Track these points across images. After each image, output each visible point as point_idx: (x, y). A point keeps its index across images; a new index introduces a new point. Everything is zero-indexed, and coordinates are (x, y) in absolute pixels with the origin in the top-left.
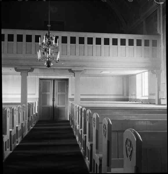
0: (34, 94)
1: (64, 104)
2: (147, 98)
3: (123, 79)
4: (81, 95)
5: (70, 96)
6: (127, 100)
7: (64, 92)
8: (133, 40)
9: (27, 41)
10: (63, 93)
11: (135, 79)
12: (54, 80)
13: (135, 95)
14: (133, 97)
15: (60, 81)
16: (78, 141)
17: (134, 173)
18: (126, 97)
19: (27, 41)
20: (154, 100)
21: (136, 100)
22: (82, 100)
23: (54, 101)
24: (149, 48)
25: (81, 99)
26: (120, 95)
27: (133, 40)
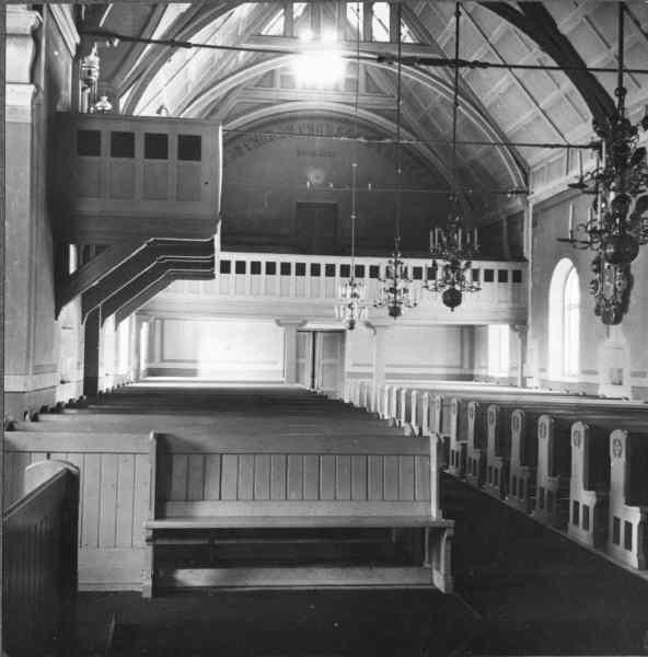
0: (275, 363)
1: (335, 384)
2: (576, 380)
3: (462, 331)
4: (388, 366)
5: (348, 367)
6: (470, 378)
7: (336, 357)
8: (492, 271)
9: (282, 273)
10: (332, 361)
11: (486, 332)
12: (314, 333)
13: (486, 367)
14: (483, 372)
15: (326, 335)
16: (444, 547)
17: (81, 588)
18: (468, 372)
19: (282, 273)
20: (516, 378)
21: (487, 379)
22: (389, 376)
23: (313, 377)
24: (228, 293)
25: (387, 375)
26: (456, 367)
27: (492, 271)
